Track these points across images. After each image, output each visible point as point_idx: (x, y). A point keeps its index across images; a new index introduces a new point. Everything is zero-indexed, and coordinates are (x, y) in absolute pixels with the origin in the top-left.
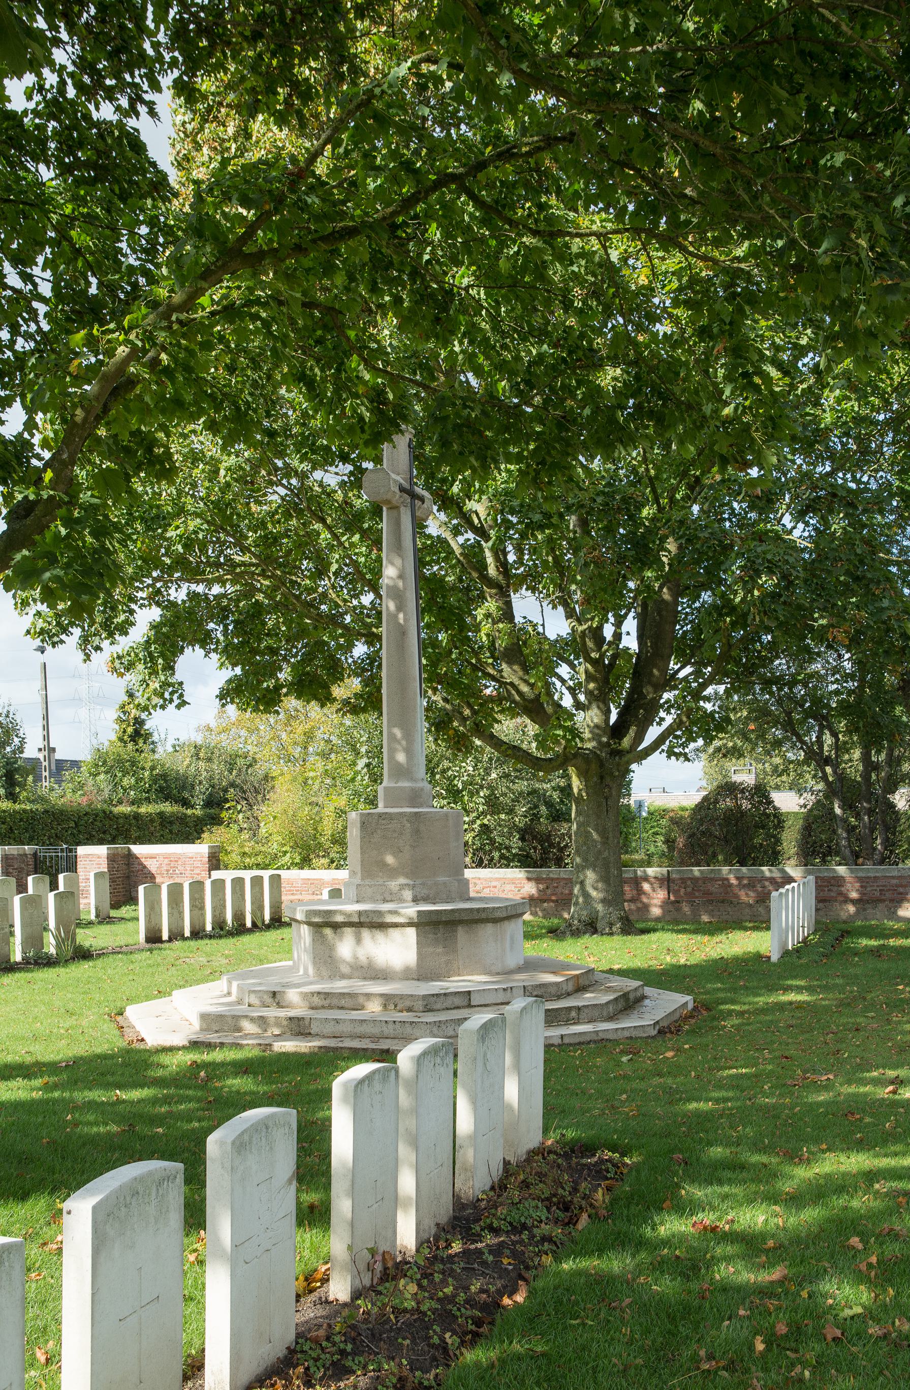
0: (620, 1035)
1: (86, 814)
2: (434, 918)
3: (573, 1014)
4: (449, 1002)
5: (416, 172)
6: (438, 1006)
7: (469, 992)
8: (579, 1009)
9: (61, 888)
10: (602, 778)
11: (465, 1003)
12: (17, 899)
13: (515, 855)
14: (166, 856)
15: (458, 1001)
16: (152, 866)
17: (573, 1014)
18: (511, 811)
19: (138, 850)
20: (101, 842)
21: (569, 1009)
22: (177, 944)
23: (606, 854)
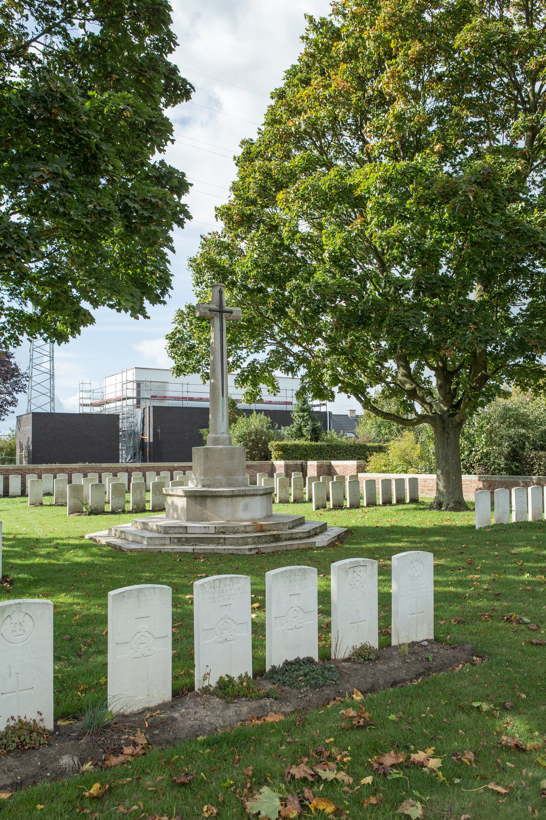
0: (227, 552)
1: (351, 446)
2: (193, 494)
3: (222, 541)
4: (176, 530)
5: (308, 133)
6: (171, 532)
7: (186, 527)
8: (225, 539)
9: (335, 480)
10: (444, 428)
11: (185, 531)
12: (330, 483)
13: (503, 468)
14: (343, 466)
15: (181, 530)
16: (338, 470)
17: (222, 541)
18: (500, 445)
19: (334, 463)
20: (352, 458)
21: (220, 538)
22: (388, 508)
23: (447, 468)
